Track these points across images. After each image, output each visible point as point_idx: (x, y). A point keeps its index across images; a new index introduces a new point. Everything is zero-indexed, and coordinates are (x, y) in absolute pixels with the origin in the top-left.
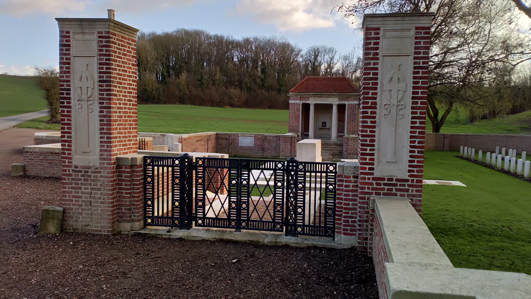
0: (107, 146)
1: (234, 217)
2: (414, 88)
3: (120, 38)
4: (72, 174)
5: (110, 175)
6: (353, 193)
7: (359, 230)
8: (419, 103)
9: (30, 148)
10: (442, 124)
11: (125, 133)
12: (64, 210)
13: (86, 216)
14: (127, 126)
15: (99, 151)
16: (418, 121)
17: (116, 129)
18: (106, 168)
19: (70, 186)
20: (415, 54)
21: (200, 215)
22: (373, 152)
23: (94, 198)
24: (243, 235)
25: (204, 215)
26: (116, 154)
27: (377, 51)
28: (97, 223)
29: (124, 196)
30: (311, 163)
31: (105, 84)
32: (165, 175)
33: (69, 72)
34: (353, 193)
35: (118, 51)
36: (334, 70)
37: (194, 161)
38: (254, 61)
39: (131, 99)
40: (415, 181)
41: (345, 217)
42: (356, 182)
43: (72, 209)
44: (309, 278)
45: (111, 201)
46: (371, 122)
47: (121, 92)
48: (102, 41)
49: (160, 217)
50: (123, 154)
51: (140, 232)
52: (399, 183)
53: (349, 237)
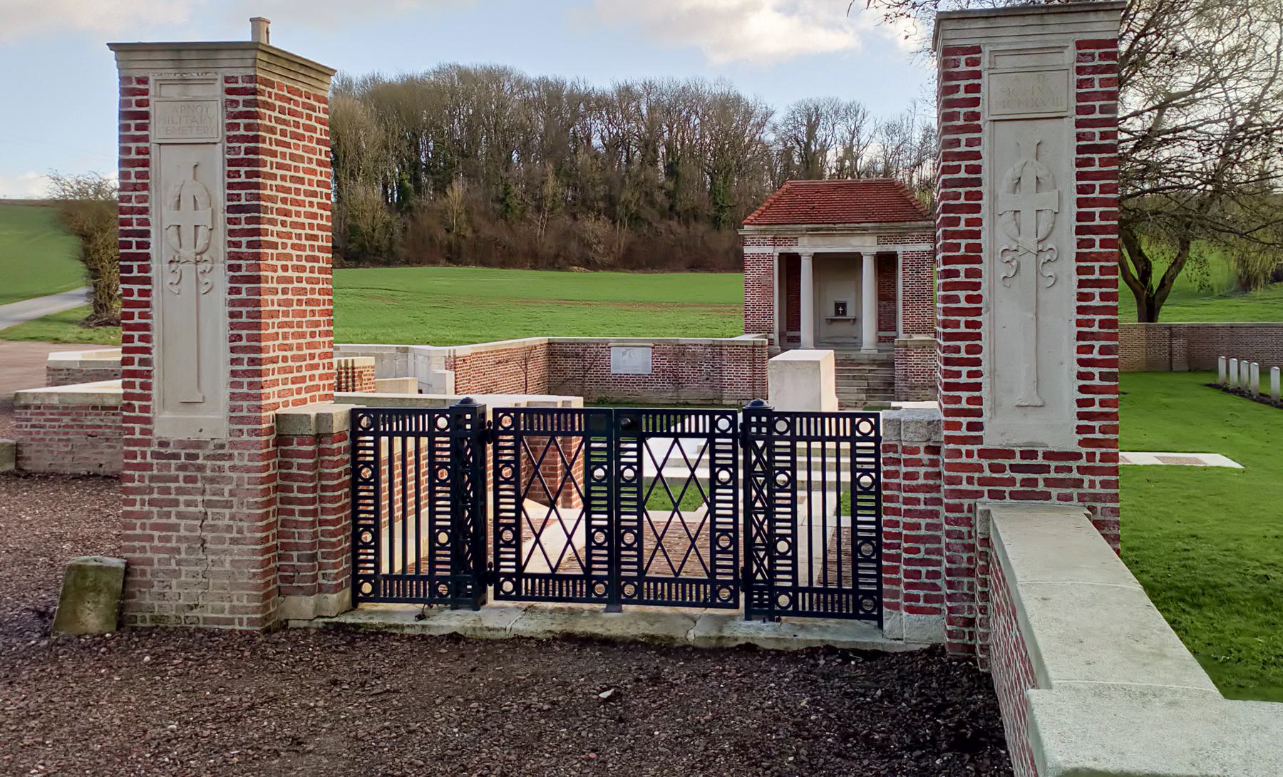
1: (600, 570)
2: (1080, 203)
3: (285, 93)
4: (152, 465)
5: (257, 464)
6: (928, 495)
7: (950, 598)
8: (1097, 243)
9: (35, 396)
10: (1163, 300)
11: (299, 347)
12: (128, 565)
13: (190, 580)
14: (304, 329)
15: (227, 397)
16: (1097, 291)
18: (246, 445)
19: (146, 497)
20: (1078, 113)
21: (508, 567)
22: (978, 380)
23: (214, 528)
25: (520, 568)
26: (276, 406)
27: (976, 109)
29: (296, 521)
30: (809, 415)
31: (243, 216)
32: (411, 458)
33: (145, 187)
34: (928, 495)
35: (279, 127)
36: (862, 164)
37: (489, 417)
38: (646, 146)
39: (317, 253)
40: (1098, 457)
41: (908, 562)
42: (934, 463)
43: (150, 562)
44: (816, 738)
47: (289, 236)
48: (237, 102)
49: (398, 578)
50: (295, 403)
51: (342, 619)
52: (1053, 464)
53: (923, 617)
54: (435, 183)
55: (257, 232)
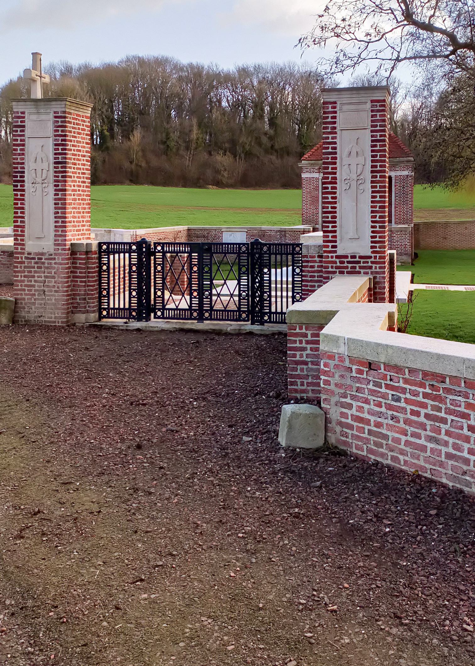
0: (62, 231)
2: (372, 161)
6: (319, 274)
8: (378, 177)
12: (16, 299)
13: (39, 306)
16: (378, 195)
17: (71, 213)
18: (60, 254)
19: (23, 274)
20: (371, 127)
21: (159, 306)
22: (335, 229)
23: (48, 286)
24: (207, 325)
27: (335, 125)
28: (51, 313)
31: (60, 165)
33: (23, 154)
34: (319, 274)
35: (73, 130)
37: (152, 246)
38: (256, 106)
40: (378, 258)
43: (24, 299)
45: (65, 289)
46: (332, 198)
47: (75, 173)
48: (58, 121)
51: (96, 323)
52: (362, 260)
54: (122, 132)
55: (65, 172)
